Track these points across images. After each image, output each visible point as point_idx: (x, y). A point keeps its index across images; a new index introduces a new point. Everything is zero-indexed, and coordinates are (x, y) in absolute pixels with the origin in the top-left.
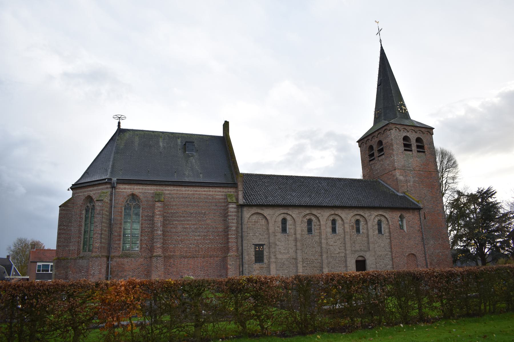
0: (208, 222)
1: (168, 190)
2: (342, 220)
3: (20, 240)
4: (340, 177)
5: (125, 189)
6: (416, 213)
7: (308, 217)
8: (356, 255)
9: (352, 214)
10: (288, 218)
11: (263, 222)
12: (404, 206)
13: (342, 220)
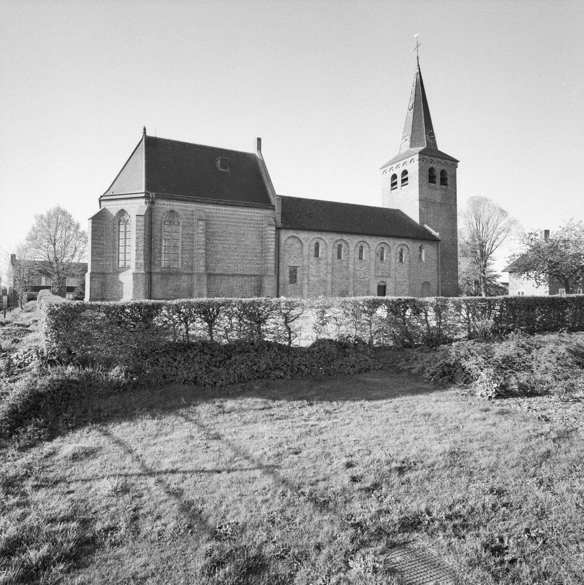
0: (247, 243)
1: (208, 209)
2: (369, 247)
7: (339, 243)
9: (379, 242)
10: (365, 245)
11: (298, 245)
13: (369, 247)
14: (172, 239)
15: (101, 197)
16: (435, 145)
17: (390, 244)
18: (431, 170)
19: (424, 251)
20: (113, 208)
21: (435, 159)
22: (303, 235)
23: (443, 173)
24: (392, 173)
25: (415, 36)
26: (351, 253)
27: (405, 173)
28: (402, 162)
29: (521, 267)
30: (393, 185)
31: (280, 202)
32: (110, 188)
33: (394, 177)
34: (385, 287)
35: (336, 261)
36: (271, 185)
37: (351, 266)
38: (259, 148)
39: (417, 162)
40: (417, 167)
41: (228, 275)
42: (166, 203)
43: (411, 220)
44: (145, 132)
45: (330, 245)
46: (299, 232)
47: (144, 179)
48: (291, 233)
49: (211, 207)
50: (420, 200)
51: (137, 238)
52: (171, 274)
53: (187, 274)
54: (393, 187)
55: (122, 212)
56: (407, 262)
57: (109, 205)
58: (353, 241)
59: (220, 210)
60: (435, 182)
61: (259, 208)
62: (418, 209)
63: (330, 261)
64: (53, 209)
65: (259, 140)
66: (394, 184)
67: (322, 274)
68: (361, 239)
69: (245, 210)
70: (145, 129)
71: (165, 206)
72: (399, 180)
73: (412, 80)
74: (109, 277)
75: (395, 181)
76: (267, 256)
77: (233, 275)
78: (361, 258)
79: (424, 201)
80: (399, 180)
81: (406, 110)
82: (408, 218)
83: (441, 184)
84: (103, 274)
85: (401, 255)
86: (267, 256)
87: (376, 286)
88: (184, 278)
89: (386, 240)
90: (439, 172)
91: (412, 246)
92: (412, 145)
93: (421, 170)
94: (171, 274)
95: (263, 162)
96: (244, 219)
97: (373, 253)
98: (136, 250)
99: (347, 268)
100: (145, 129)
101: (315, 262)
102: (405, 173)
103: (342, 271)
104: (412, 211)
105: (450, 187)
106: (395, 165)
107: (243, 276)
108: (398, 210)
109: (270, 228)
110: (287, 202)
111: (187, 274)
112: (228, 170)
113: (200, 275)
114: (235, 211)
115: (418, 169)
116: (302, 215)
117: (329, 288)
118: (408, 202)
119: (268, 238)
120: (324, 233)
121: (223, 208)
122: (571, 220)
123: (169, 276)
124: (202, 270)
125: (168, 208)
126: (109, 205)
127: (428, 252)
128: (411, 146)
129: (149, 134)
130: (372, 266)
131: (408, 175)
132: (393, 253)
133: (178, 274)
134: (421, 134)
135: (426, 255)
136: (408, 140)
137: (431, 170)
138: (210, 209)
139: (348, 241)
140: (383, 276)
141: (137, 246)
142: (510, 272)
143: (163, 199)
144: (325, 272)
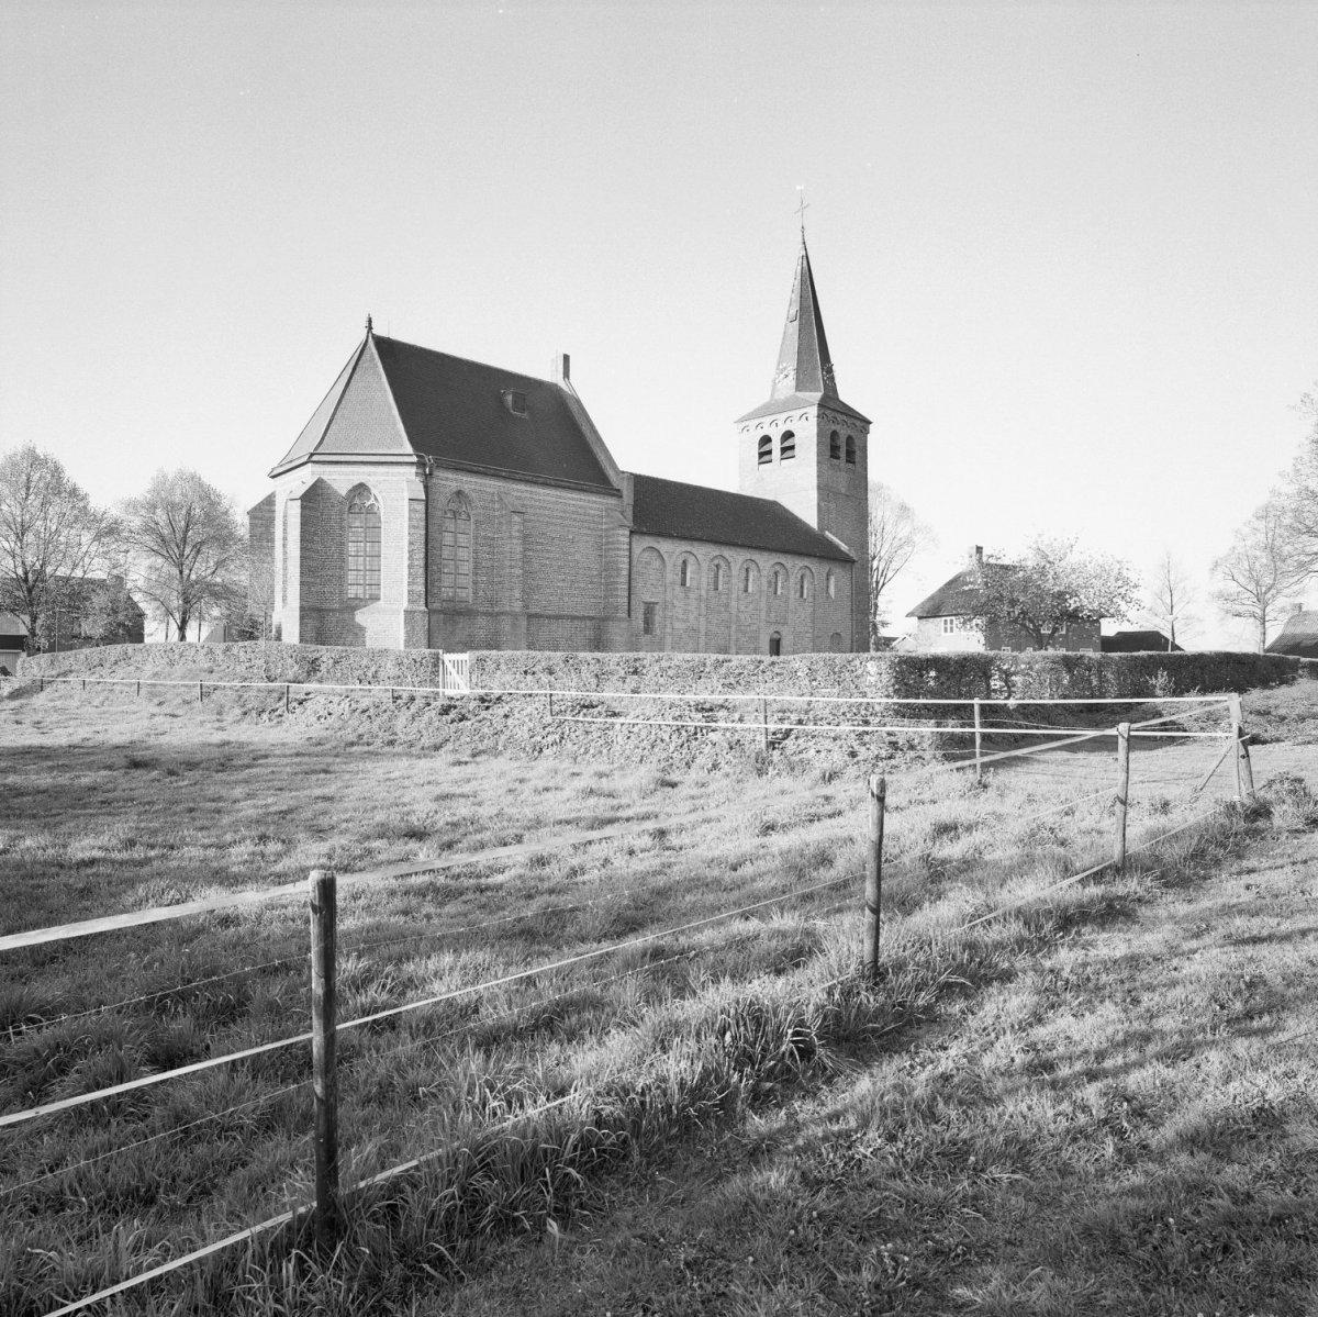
0: (577, 557)
1: (518, 490)
2: (759, 571)
3: (194, 479)
4: (713, 487)
5: (447, 479)
6: (848, 565)
7: (716, 562)
8: (771, 630)
9: (772, 562)
10: (691, 560)
11: (657, 564)
12: (844, 560)
13: (759, 571)
14: (461, 545)
15: (312, 455)
16: (835, 391)
17: (788, 566)
18: (834, 434)
19: (832, 579)
20: (341, 480)
21: (840, 417)
22: (665, 546)
23: (850, 439)
24: (761, 433)
25: (798, 188)
26: (734, 581)
27: (789, 435)
28: (785, 415)
29: (932, 610)
30: (761, 455)
31: (632, 484)
32: (323, 439)
33: (766, 440)
34: (252, 637)
35: (712, 593)
36: (606, 451)
37: (734, 603)
38: (566, 374)
39: (813, 421)
40: (814, 430)
41: (549, 617)
42: (450, 476)
43: (805, 524)
44: (370, 328)
45: (705, 565)
46: (660, 539)
47: (400, 426)
48: (648, 541)
49: (522, 487)
50: (819, 488)
51: (411, 543)
52: (460, 613)
53: (485, 614)
54: (763, 459)
55: (361, 489)
56: (811, 599)
57: (330, 473)
58: (738, 557)
59: (375, 474)
60: (838, 458)
61: (598, 493)
62: (815, 502)
63: (703, 593)
64: (20, 449)
65: (566, 358)
66: (764, 455)
67: (691, 617)
68: (689, 548)
69: (575, 495)
70: (370, 321)
71: (450, 481)
72: (776, 446)
73: (792, 270)
74: (332, 618)
75: (766, 448)
76: (617, 583)
77: (558, 617)
78: (746, 591)
79: (825, 490)
80: (776, 446)
81: (782, 320)
82: (786, 511)
83: (848, 461)
84: (319, 610)
85: (684, 572)
86: (617, 583)
87: (767, 639)
88: (481, 621)
89: (782, 559)
90: (844, 439)
91: (818, 568)
92: (800, 385)
93: (820, 434)
94: (460, 613)
95: (578, 402)
96: (573, 513)
97: (764, 581)
98: (410, 567)
99: (727, 606)
100: (370, 321)
101: (682, 595)
102: (789, 435)
103: (719, 612)
104: (804, 504)
105: (858, 466)
106: (768, 419)
107: (574, 618)
108: (774, 503)
109: (621, 532)
110: (643, 485)
111: (485, 614)
112: (525, 415)
113: (515, 616)
114: (531, 492)
115: (815, 431)
116: (668, 510)
117: (702, 640)
118: (796, 487)
119: (618, 549)
120: (696, 544)
121: (541, 490)
122: (1040, 535)
123: (456, 618)
124: (517, 606)
125: (454, 486)
126: (330, 473)
127: (837, 583)
128: (798, 388)
129: (378, 331)
130: (763, 605)
131: (796, 441)
132: (792, 580)
133: (469, 613)
134: (815, 368)
135: (836, 586)
136: (791, 377)
137: (834, 434)
138: (519, 491)
139: (730, 559)
140: (777, 622)
141: (410, 558)
142: (920, 618)
143: (447, 468)
144: (696, 614)
